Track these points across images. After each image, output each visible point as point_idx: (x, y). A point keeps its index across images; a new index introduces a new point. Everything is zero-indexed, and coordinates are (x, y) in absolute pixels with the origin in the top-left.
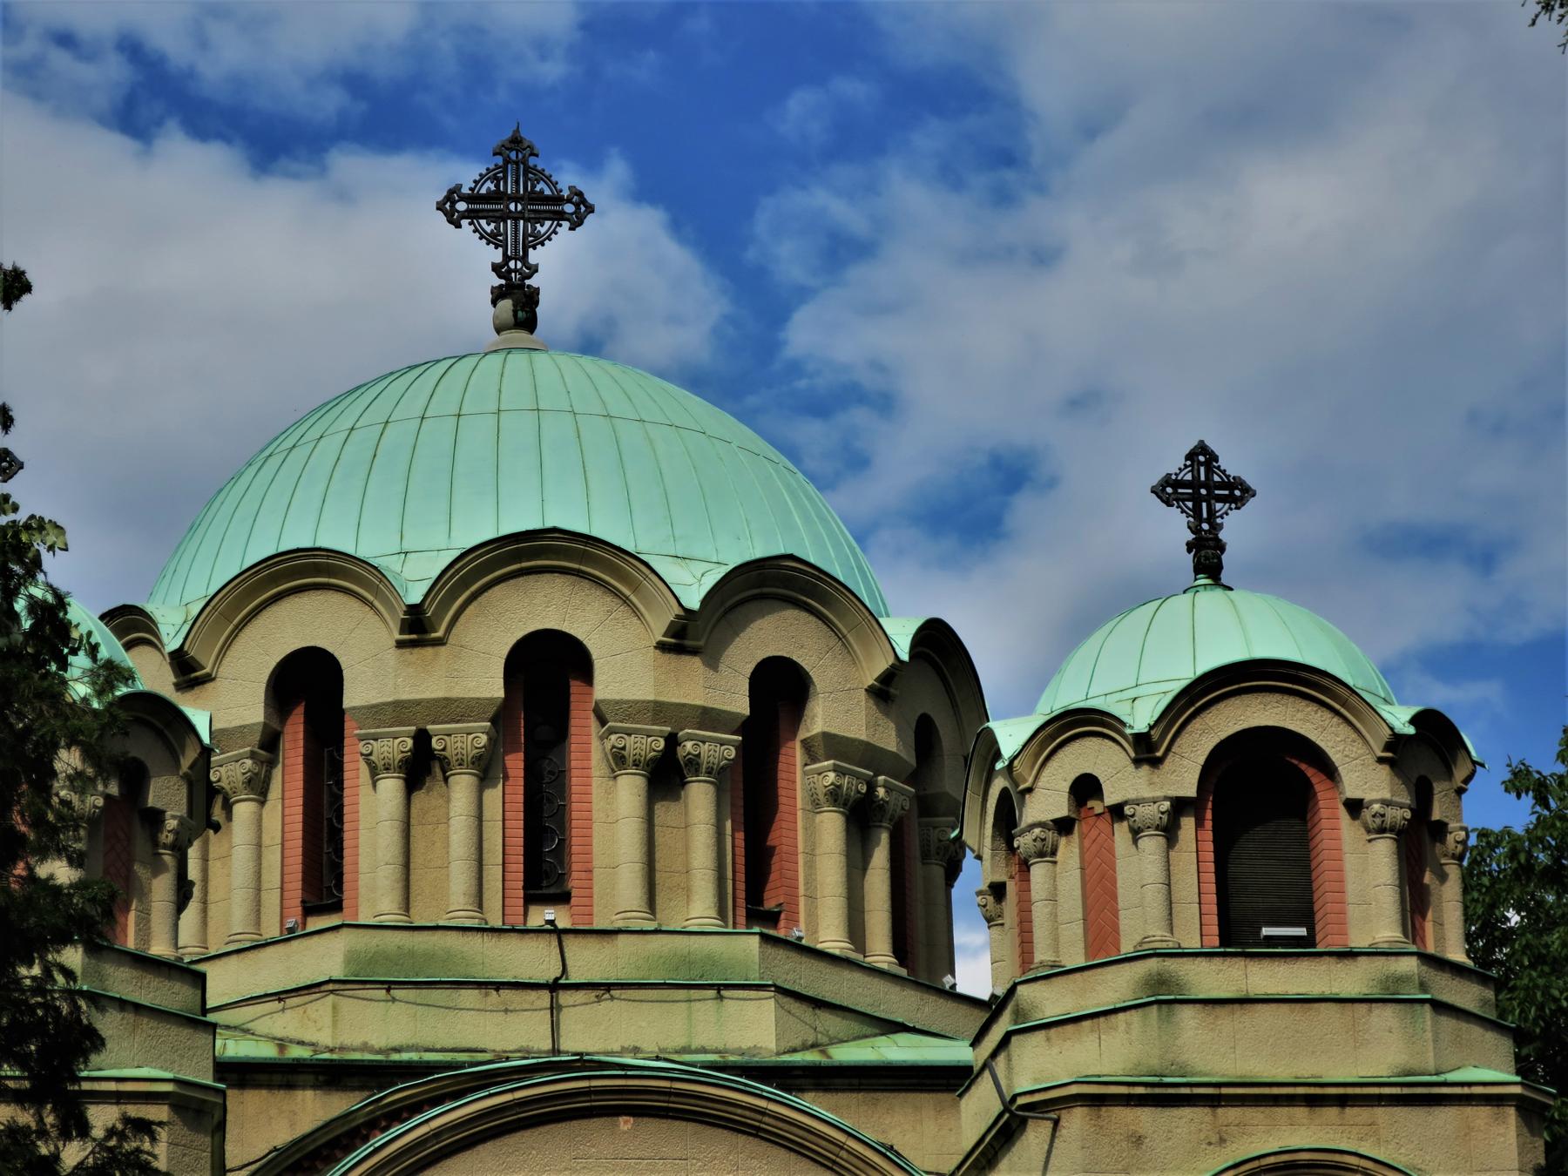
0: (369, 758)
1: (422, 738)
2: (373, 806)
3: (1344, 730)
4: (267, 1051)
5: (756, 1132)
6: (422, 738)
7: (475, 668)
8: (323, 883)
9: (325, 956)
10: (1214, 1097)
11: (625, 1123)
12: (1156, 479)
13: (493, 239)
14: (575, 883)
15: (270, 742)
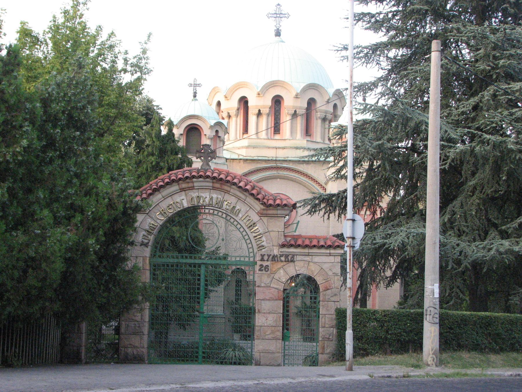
1: (259, 111)
2: (252, 119)
4: (236, 157)
5: (295, 181)
6: (259, 111)
7: (268, 102)
8: (246, 130)
9: (245, 143)
11: (278, 180)
14: (281, 131)
15: (238, 109)
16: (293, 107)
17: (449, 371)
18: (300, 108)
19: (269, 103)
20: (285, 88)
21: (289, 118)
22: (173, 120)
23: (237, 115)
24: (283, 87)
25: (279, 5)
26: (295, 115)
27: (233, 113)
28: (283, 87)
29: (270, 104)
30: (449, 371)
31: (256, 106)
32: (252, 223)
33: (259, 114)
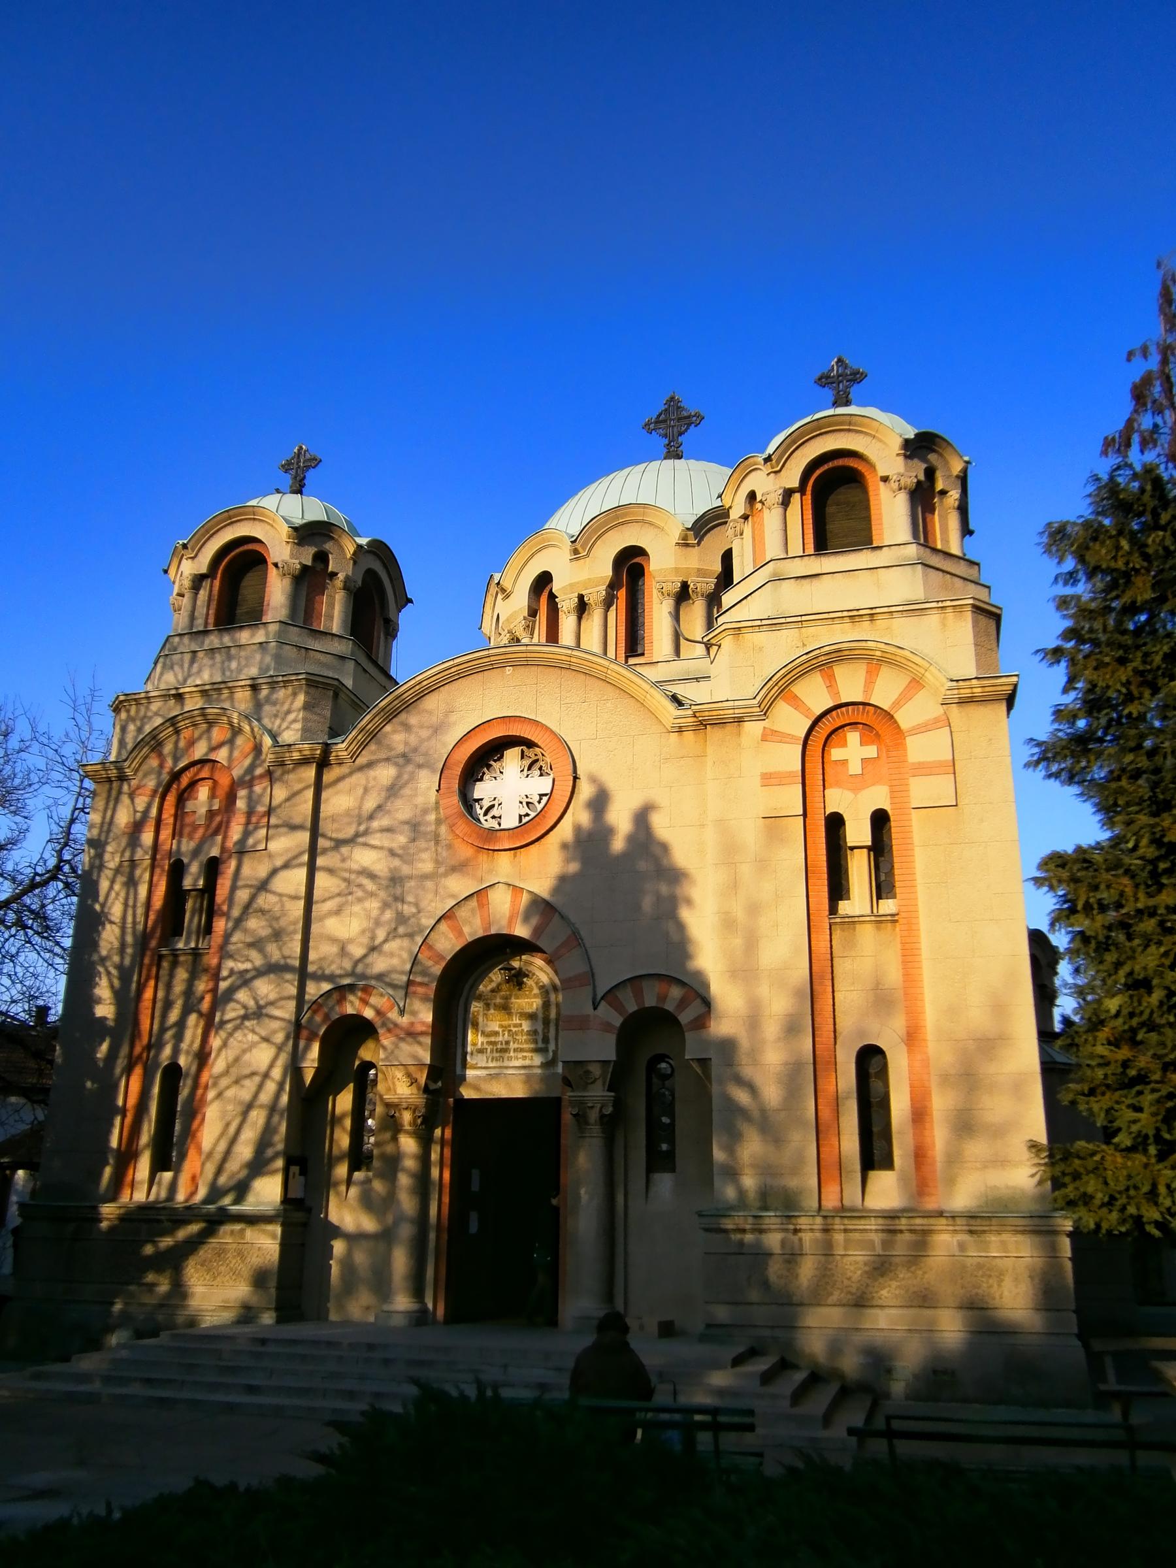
0: (566, 604)
1: (581, 597)
3: (862, 436)
6: (581, 597)
7: (600, 566)
10: (801, 621)
11: (509, 670)
12: (817, 376)
13: (665, 436)
16: (677, 570)
17: (219, 576)
18: (701, 572)
19: (606, 571)
20: (651, 524)
21: (668, 605)
22: (1060, 631)
23: (608, 602)
24: (643, 522)
25: (672, 399)
26: (683, 595)
27: (596, 594)
28: (643, 522)
29: (611, 574)
30: (219, 576)
31: (571, 585)
32: (972, 1222)
33: (582, 607)
